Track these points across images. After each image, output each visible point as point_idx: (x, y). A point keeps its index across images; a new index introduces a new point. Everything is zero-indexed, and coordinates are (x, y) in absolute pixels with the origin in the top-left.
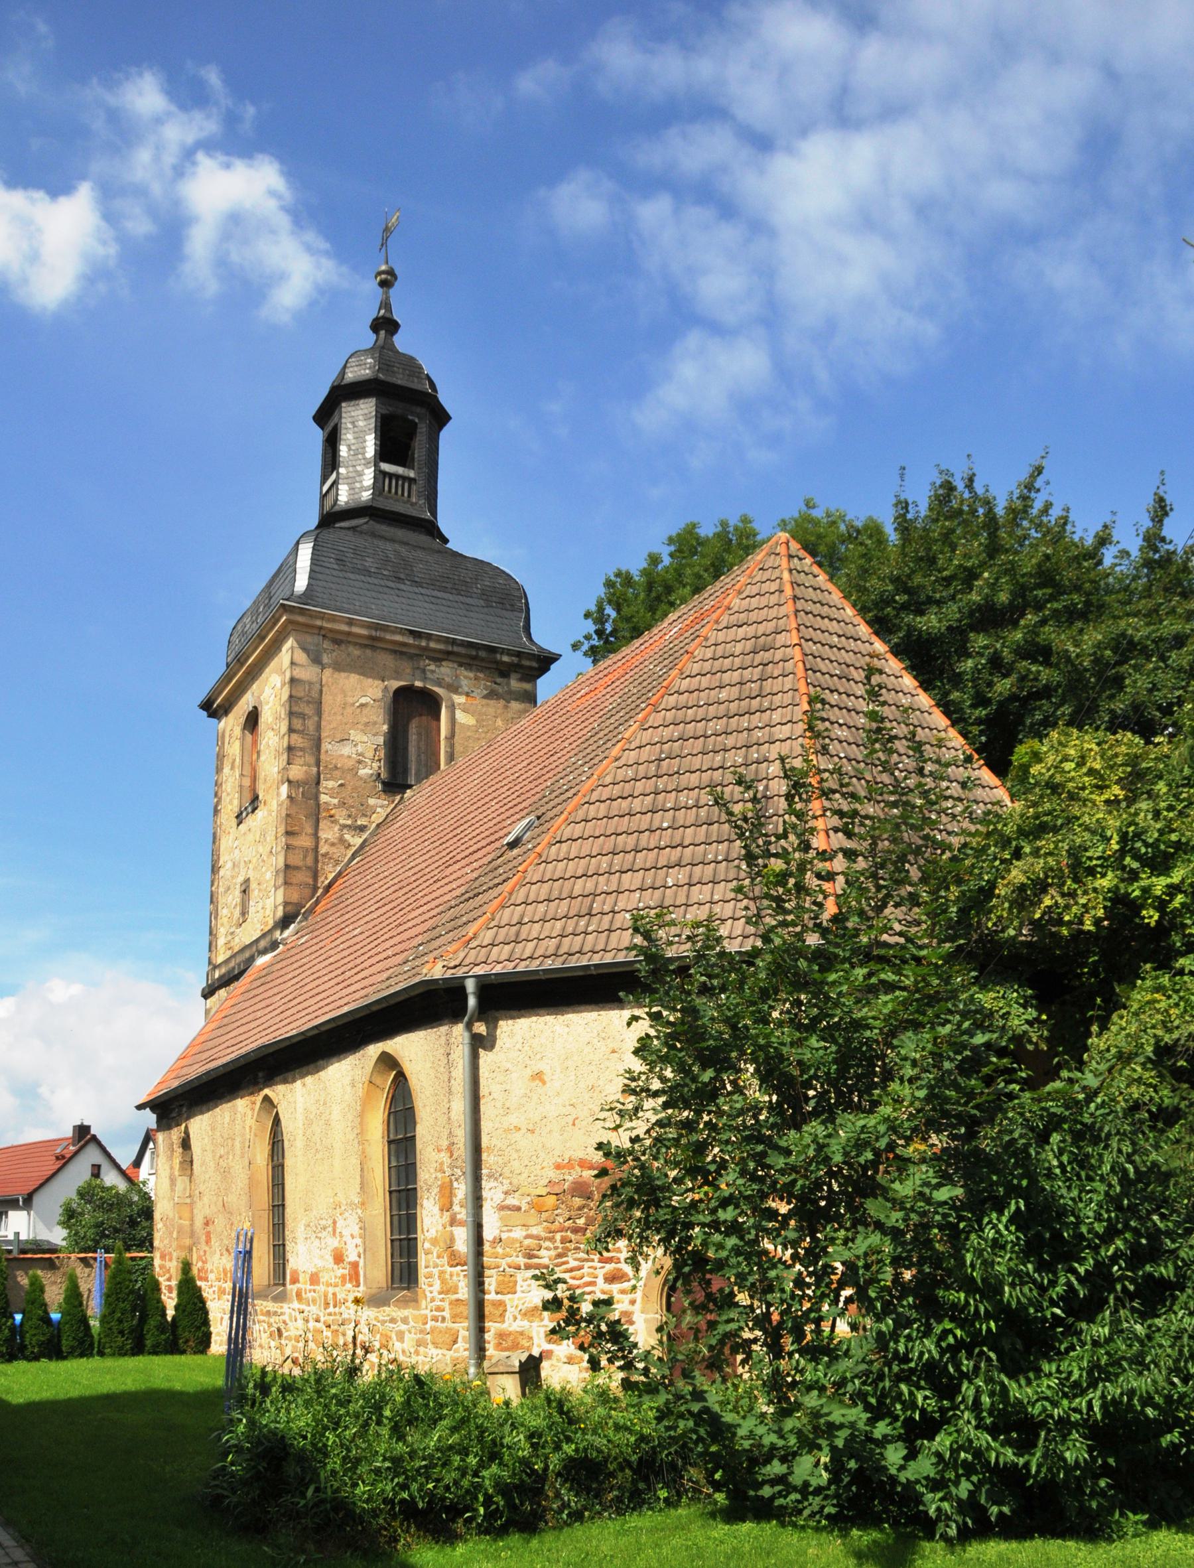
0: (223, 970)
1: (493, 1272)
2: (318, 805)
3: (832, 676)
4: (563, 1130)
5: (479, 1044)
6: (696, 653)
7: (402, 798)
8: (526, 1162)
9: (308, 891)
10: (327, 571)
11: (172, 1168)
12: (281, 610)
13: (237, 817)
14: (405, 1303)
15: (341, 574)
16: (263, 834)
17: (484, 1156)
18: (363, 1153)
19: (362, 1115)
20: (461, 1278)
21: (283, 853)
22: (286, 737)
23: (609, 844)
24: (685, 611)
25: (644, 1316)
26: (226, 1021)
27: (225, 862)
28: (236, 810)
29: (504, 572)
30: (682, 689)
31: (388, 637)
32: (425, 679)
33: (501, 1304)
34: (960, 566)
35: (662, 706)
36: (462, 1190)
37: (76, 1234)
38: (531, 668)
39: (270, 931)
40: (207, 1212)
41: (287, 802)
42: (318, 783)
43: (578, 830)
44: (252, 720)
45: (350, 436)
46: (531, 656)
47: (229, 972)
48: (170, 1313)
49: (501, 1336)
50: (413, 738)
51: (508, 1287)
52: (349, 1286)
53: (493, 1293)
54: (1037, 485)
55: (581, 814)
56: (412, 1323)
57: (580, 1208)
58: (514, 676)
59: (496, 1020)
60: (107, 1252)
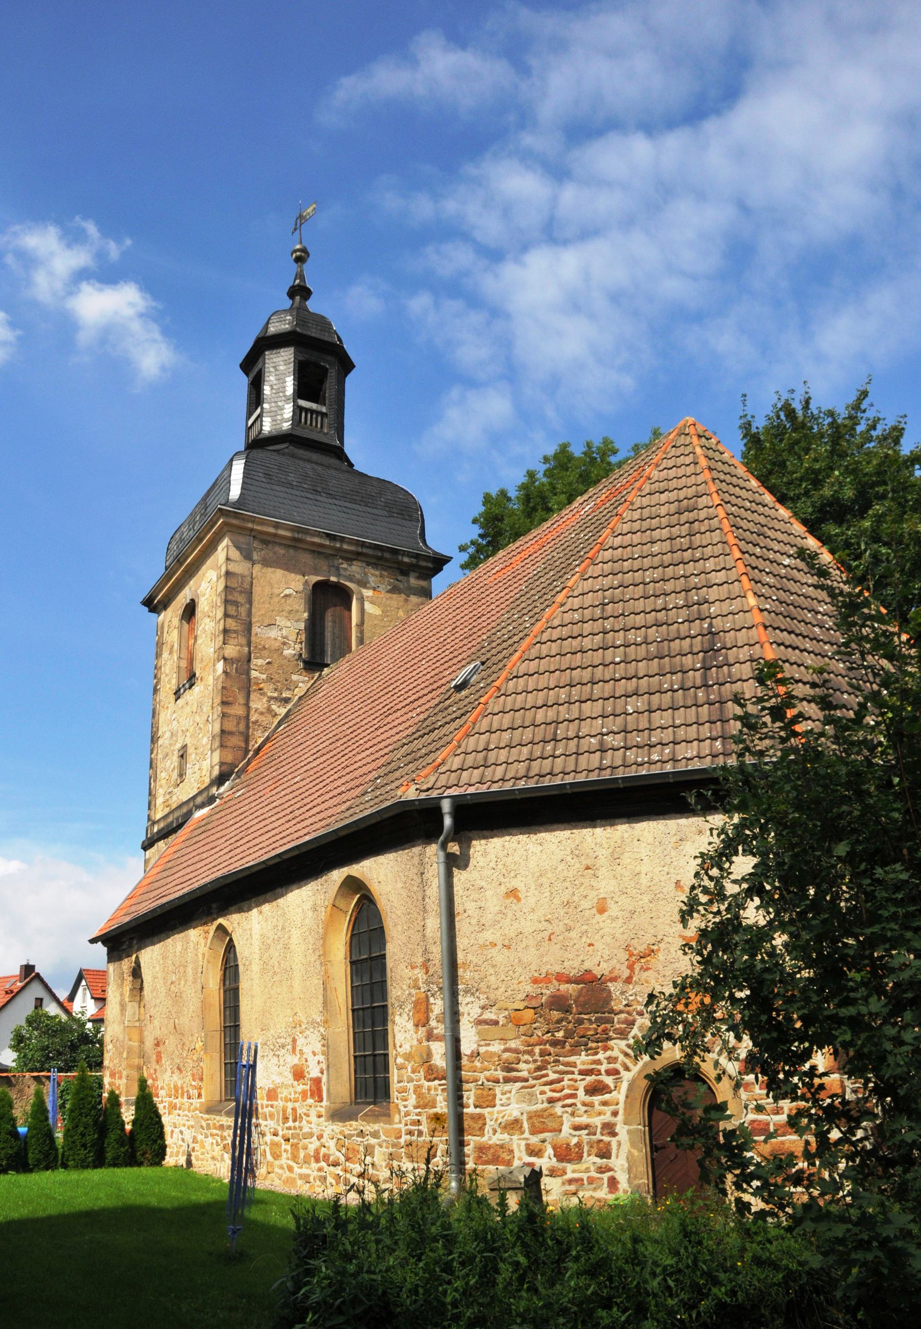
0: (162, 825)
1: (472, 1086)
2: (249, 680)
3: (752, 533)
4: (538, 945)
5: (454, 863)
6: (624, 515)
7: (320, 675)
8: (503, 977)
9: (240, 753)
10: (257, 483)
11: (122, 995)
12: (219, 514)
13: (175, 694)
14: (374, 1117)
15: (268, 486)
16: (200, 706)
17: (460, 972)
18: (326, 973)
19: (324, 938)
20: (439, 1092)
21: (219, 720)
22: (222, 622)
23: (565, 677)
24: (513, 548)
25: (626, 1127)
26: (170, 865)
27: (164, 733)
28: (175, 688)
29: (403, 489)
30: (615, 545)
31: (309, 539)
32: (338, 575)
33: (481, 1117)
34: (810, 468)
35: (599, 559)
36: (438, 1005)
37: (24, 1056)
38: (427, 568)
39: (207, 788)
40: (158, 1033)
41: (223, 676)
42: (249, 661)
43: (533, 666)
44: (190, 611)
45: (272, 378)
46: (427, 558)
47: (168, 826)
48: (128, 1127)
49: (481, 1149)
50: (329, 625)
51: (487, 1100)
52: (310, 1101)
53: (472, 1107)
54: (863, 407)
55: (534, 652)
56: (383, 1137)
57: (559, 1021)
58: (412, 574)
59: (471, 840)
60: (59, 1071)
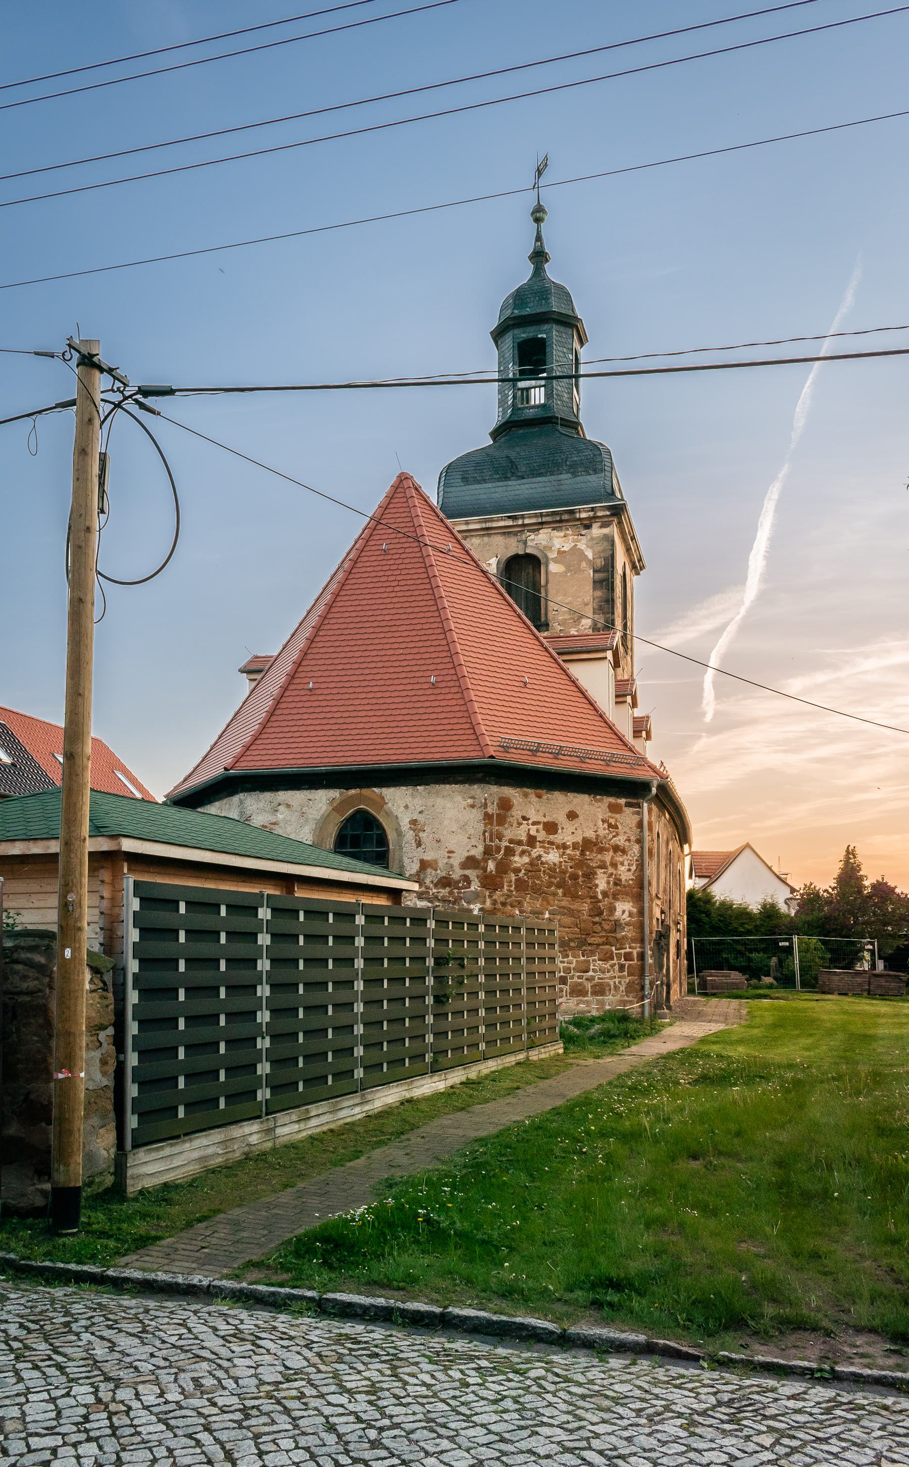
58: (595, 526)
